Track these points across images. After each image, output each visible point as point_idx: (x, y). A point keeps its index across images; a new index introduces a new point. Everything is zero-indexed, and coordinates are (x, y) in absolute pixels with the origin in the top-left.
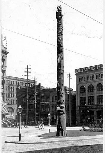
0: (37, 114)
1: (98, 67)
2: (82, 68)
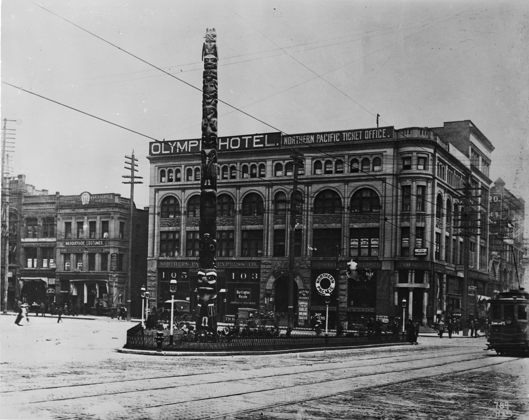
1: (220, 144)
2: (172, 142)
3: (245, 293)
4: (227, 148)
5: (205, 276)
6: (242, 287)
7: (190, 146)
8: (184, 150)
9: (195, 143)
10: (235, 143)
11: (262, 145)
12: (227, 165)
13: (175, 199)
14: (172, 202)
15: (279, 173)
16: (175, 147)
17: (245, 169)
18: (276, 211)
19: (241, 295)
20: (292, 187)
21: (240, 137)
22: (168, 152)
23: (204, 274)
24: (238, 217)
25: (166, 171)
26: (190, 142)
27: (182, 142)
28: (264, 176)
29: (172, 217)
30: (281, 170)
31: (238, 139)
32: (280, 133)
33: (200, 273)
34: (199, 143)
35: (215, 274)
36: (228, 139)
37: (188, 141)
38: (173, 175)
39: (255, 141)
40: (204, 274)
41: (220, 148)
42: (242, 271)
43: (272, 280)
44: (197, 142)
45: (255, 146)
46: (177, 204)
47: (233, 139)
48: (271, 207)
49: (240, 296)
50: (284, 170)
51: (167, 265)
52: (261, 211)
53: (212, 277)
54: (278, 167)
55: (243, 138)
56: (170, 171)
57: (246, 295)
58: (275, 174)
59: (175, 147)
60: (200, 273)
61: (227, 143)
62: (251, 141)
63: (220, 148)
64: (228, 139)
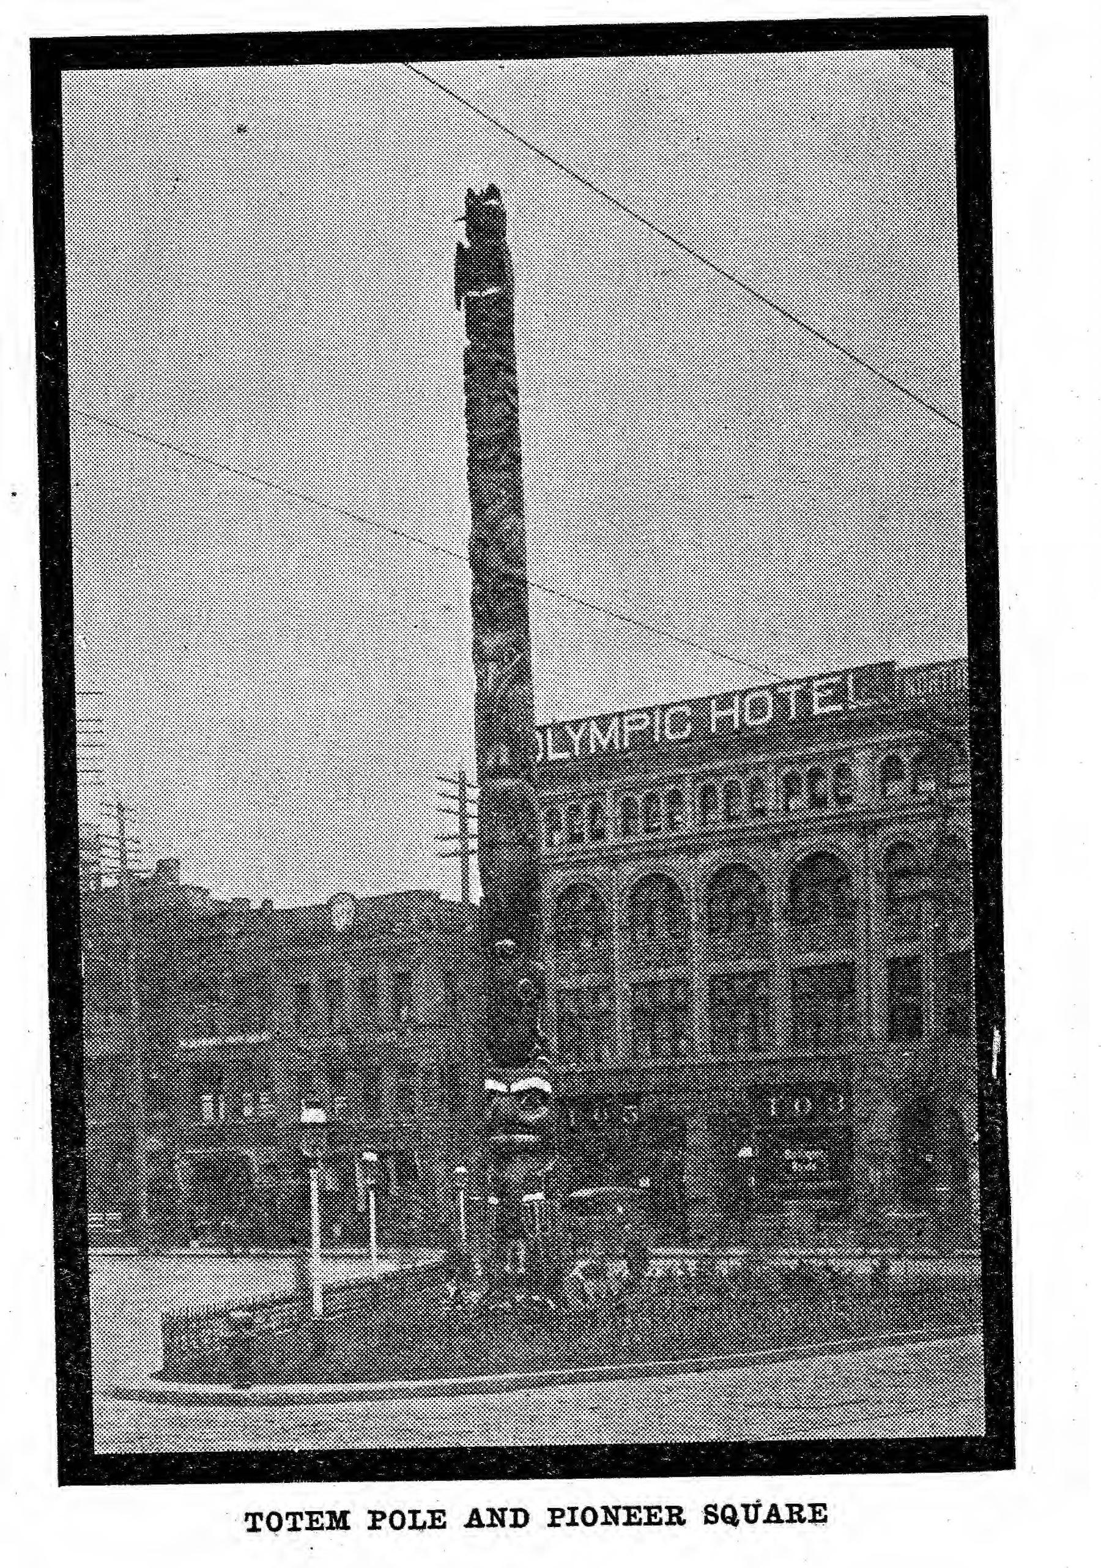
0: (154, 1143)
1: (715, 715)
2: (576, 724)
3: (809, 1155)
4: (736, 725)
5: (508, 1094)
6: (802, 1136)
7: (627, 729)
8: (611, 744)
9: (642, 721)
10: (758, 707)
11: (839, 708)
12: (712, 780)
13: (672, 886)
14: (584, 900)
15: (895, 788)
16: (584, 742)
17: (790, 785)
18: (892, 901)
19: (799, 1161)
20: (932, 826)
21: (773, 688)
22: (566, 755)
23: (502, 1087)
24: (779, 928)
25: (639, 799)
26: (626, 719)
27: (603, 722)
28: (848, 799)
29: (588, 945)
30: (900, 776)
31: (766, 693)
32: (891, 664)
33: (490, 1084)
34: (652, 721)
35: (547, 1087)
36: (736, 698)
37: (621, 715)
38: (583, 823)
39: (816, 695)
40: (502, 1087)
41: (713, 729)
42: (798, 1090)
43: (889, 1109)
44: (645, 716)
45: (817, 710)
46: (597, 906)
47: (672, 711)
48: (876, 890)
49: (795, 1166)
50: (909, 778)
51: (580, 1087)
52: (756, 911)
53: (534, 1097)
54: (890, 769)
55: (780, 690)
56: (815, 775)
57: (813, 1161)
58: (884, 791)
59: (584, 742)
60: (490, 1084)
61: (735, 712)
62: (804, 697)
63: (713, 729)
64: (736, 698)
